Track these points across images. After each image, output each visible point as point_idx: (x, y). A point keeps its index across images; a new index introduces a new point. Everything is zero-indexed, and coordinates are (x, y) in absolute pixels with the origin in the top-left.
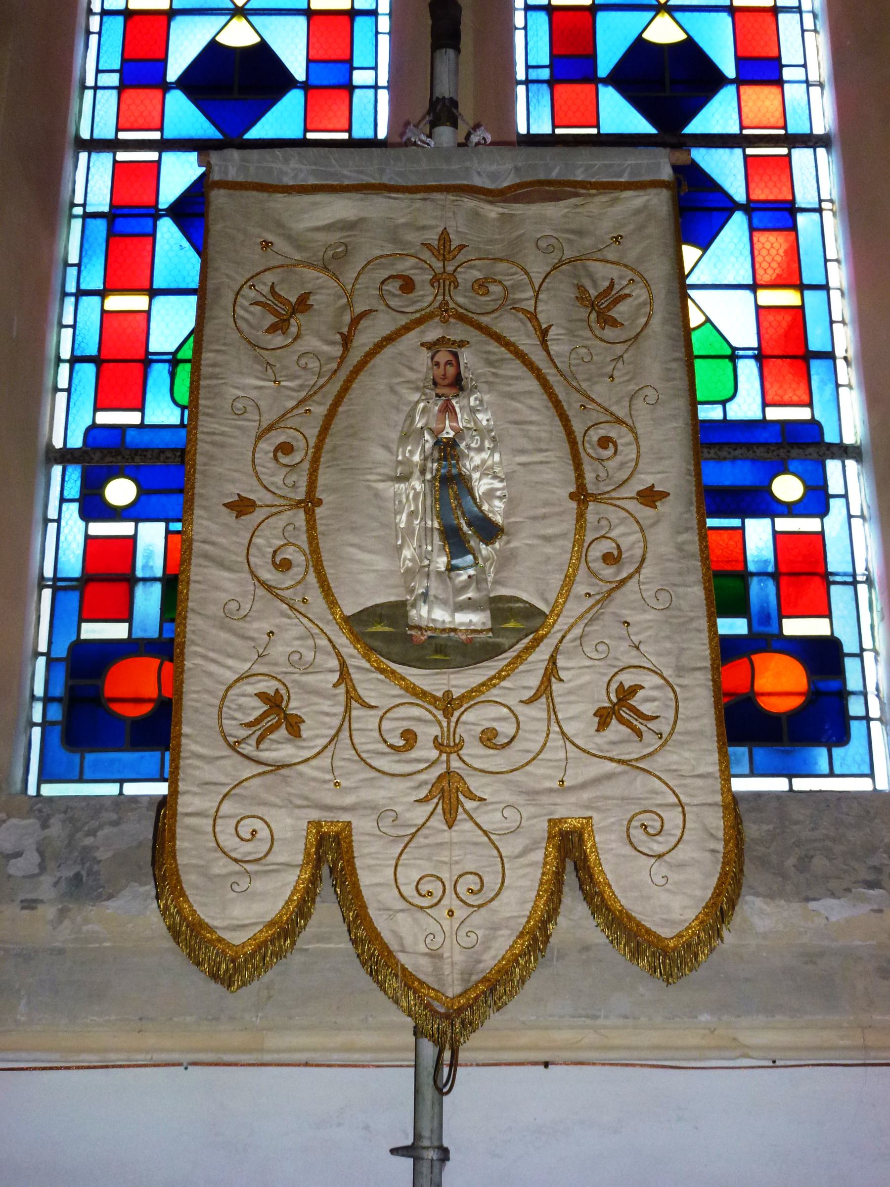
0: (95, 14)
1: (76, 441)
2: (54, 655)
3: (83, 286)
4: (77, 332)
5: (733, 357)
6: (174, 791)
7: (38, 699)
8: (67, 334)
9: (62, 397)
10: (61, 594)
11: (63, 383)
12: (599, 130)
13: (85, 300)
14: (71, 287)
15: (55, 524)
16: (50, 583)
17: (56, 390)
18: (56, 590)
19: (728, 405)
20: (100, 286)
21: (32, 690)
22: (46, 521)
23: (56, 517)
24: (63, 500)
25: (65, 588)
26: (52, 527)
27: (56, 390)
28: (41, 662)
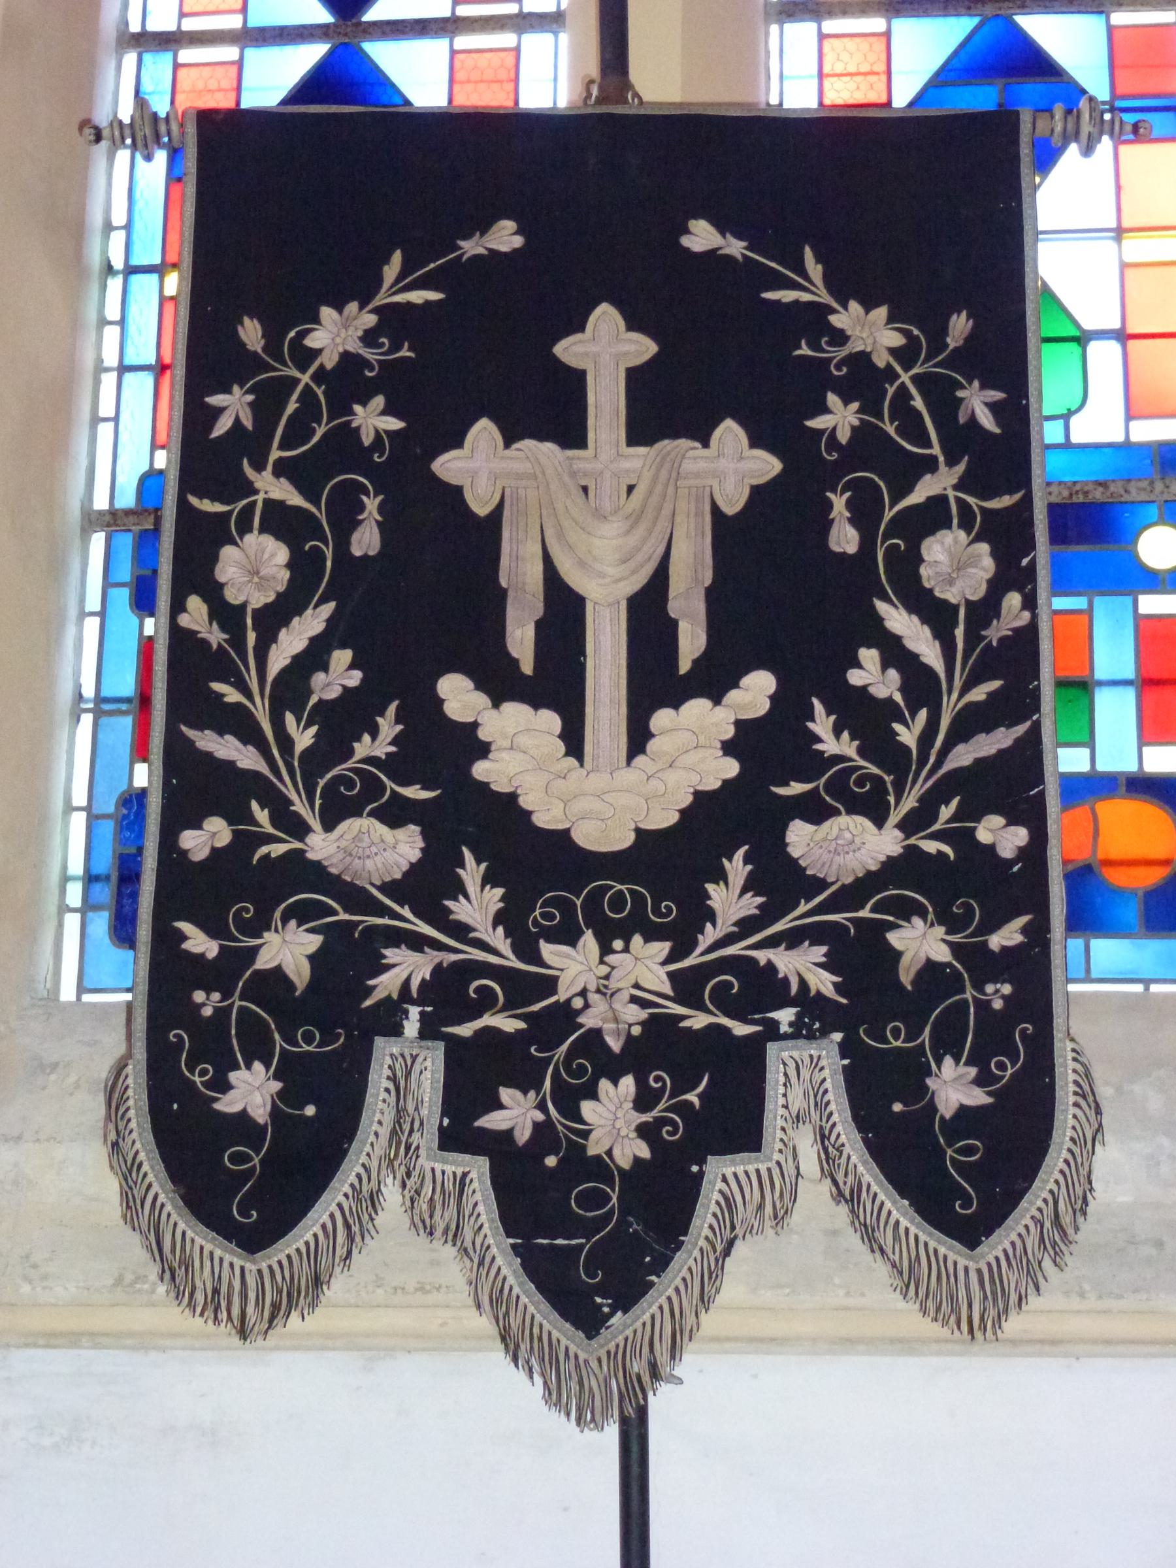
0: (118, 272)
1: (127, 499)
2: (96, 810)
3: (134, 261)
4: (135, 237)
5: (1082, 339)
6: (786, 1037)
7: (74, 878)
8: (111, 334)
9: (92, 626)
10: (104, 720)
11: (112, 311)
12: (819, 29)
13: (135, 279)
14: (111, 358)
15: (111, 424)
16: (91, 705)
17: (103, 322)
18: (98, 714)
19: (1074, 421)
20: (157, 260)
21: (65, 867)
22: (96, 420)
23: (112, 415)
24: (108, 584)
25: (111, 713)
26: (105, 431)
27: (103, 322)
28: (79, 821)
